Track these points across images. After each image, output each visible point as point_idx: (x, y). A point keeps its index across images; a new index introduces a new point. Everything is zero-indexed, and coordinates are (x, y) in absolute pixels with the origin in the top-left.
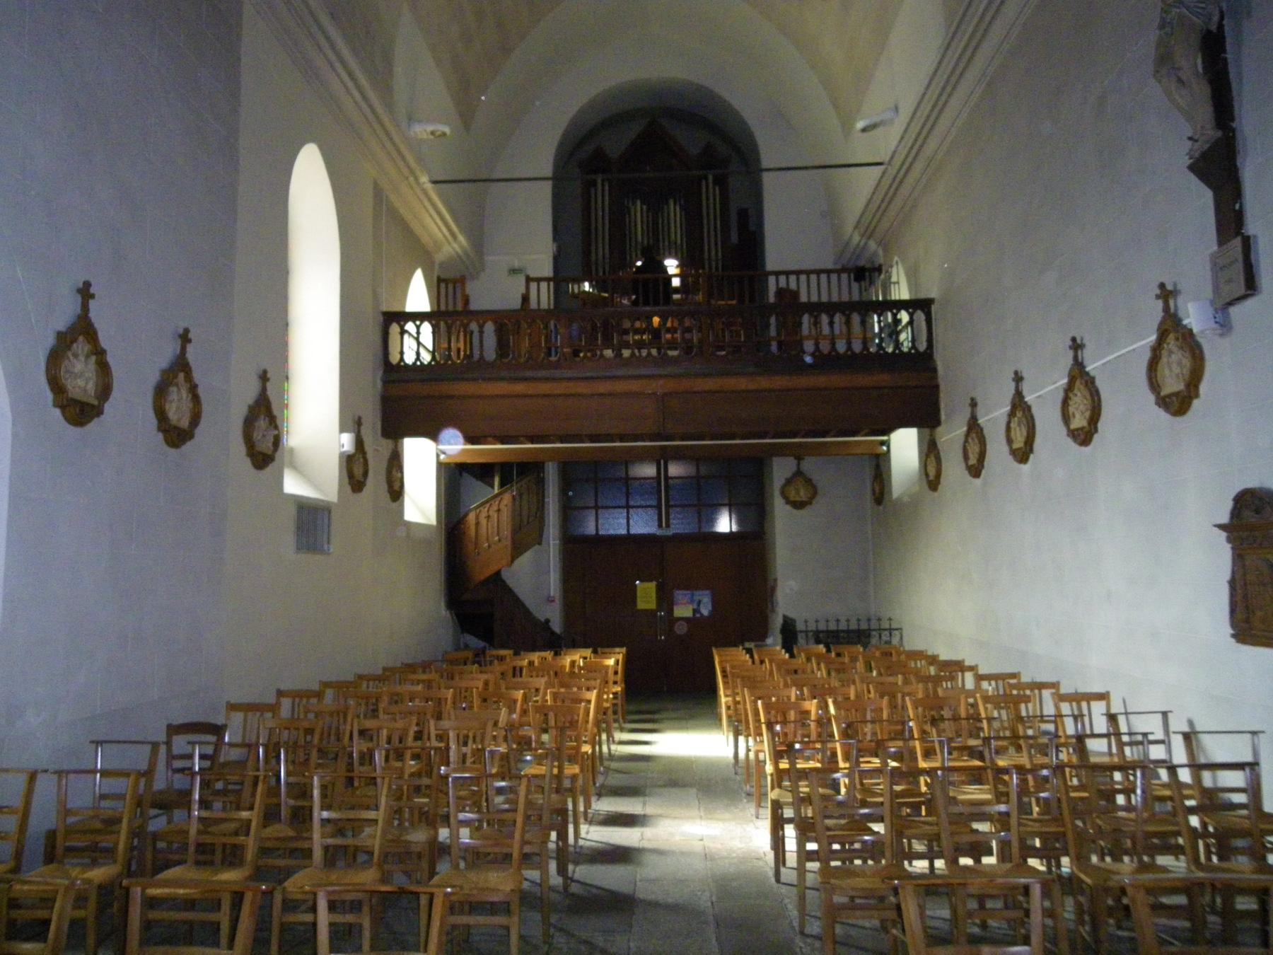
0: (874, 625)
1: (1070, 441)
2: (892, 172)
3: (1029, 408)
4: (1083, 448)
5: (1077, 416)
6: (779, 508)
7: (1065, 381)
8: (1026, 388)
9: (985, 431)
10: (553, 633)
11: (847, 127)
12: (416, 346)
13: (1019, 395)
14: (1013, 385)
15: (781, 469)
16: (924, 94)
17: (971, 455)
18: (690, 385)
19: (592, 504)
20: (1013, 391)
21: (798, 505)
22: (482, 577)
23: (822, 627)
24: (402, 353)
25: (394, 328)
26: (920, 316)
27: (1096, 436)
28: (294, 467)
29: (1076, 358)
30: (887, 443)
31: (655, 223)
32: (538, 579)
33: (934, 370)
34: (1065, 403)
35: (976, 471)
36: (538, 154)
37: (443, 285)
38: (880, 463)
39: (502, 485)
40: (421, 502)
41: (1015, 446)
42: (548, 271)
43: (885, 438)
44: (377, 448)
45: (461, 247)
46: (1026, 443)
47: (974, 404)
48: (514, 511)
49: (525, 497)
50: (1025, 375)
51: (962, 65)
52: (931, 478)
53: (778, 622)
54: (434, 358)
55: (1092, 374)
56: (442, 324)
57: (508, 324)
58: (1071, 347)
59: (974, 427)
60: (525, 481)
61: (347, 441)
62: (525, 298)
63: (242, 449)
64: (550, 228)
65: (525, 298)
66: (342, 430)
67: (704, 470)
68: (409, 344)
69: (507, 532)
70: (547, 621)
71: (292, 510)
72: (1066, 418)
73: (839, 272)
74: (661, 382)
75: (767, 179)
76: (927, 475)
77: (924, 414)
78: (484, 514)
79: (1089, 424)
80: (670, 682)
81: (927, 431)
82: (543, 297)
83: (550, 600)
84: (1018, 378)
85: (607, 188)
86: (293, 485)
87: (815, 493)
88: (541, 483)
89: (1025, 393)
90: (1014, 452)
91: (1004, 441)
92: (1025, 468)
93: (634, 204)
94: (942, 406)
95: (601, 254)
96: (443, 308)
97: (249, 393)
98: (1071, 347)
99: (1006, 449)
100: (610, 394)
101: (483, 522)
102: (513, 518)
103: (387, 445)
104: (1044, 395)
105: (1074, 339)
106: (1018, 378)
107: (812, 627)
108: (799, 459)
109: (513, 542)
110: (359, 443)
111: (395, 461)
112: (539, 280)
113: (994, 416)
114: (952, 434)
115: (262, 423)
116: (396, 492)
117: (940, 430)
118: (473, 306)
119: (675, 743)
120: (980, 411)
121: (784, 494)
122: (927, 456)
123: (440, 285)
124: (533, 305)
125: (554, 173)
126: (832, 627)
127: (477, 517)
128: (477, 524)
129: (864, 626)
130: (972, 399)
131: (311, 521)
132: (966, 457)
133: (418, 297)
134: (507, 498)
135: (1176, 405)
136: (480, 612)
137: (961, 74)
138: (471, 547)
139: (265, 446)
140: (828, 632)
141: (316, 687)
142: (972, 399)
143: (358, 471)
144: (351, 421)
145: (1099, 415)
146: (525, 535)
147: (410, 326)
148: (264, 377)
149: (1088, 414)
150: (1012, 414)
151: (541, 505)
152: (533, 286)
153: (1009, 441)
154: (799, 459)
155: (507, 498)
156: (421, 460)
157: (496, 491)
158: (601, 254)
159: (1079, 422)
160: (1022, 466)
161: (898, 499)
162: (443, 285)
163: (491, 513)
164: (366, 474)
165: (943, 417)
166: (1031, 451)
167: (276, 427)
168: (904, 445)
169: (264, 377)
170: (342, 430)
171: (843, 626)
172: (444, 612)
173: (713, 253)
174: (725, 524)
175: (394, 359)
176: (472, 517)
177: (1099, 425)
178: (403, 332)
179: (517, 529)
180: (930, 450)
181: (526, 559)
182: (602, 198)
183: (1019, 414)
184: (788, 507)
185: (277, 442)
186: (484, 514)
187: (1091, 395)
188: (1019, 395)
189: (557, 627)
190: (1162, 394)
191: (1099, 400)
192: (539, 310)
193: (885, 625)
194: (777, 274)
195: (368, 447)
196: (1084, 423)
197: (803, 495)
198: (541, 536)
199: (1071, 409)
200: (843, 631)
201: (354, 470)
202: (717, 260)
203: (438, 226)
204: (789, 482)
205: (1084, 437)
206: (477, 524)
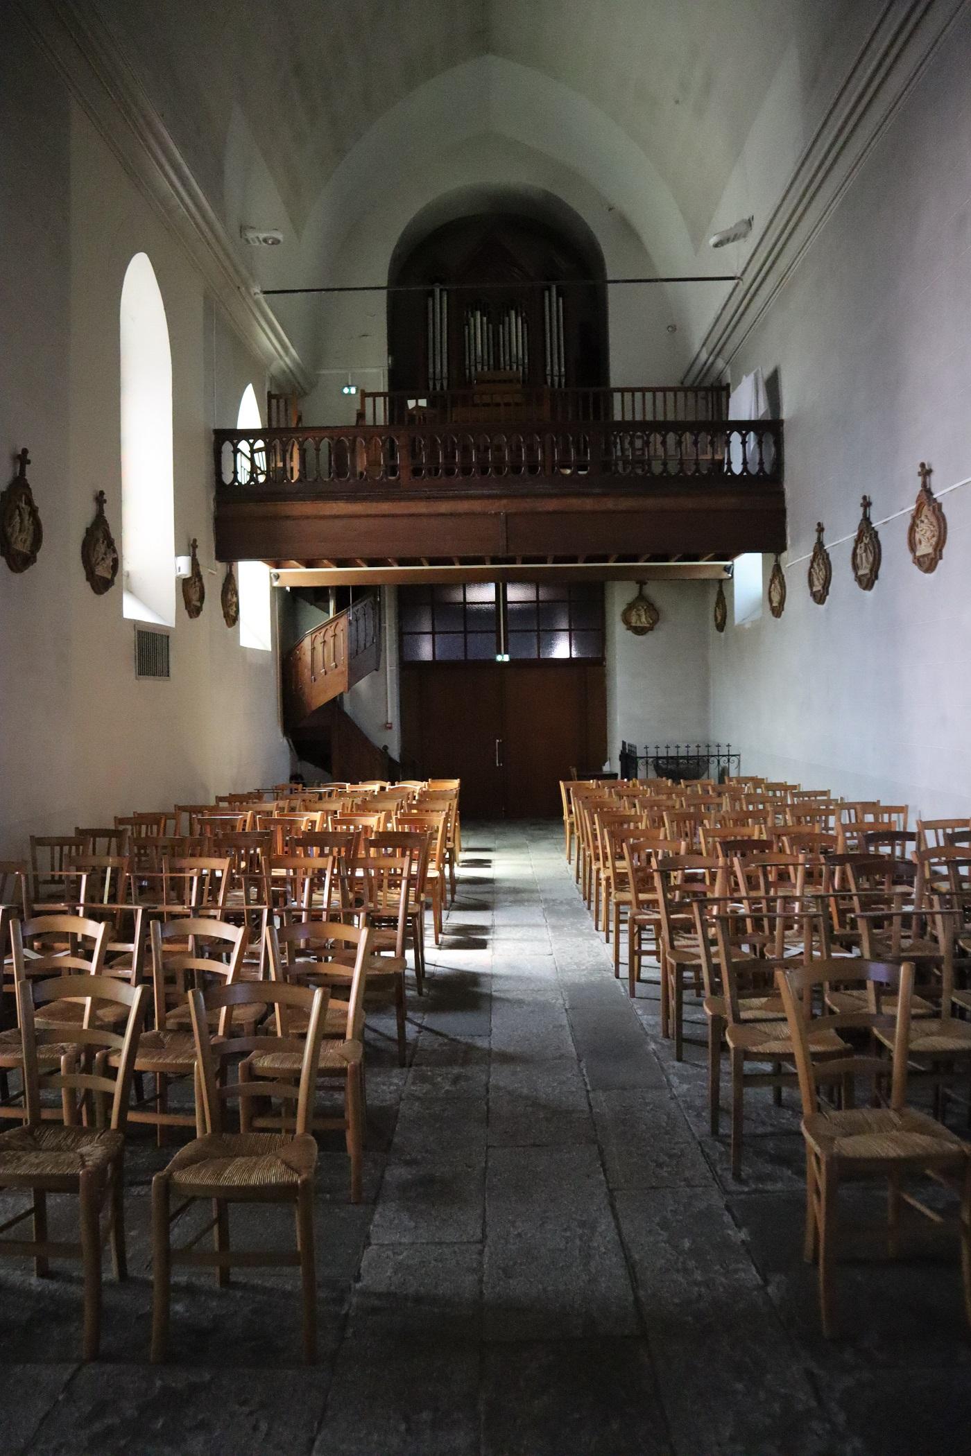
0: (714, 751)
1: (915, 568)
2: (743, 286)
3: (876, 533)
4: (927, 575)
5: (923, 543)
6: (619, 633)
7: (914, 507)
8: (935, 482)
9: (831, 557)
10: (391, 760)
11: (697, 238)
12: (246, 465)
13: (866, 520)
14: (815, 535)
15: (619, 597)
16: (780, 206)
17: (816, 582)
18: (537, 465)
19: (429, 629)
20: (861, 517)
21: (639, 631)
22: (314, 708)
23: (663, 753)
24: (235, 473)
25: (227, 447)
26: (769, 439)
27: (940, 562)
28: (131, 592)
29: (924, 484)
30: (728, 569)
31: (496, 334)
32: (379, 707)
33: (781, 494)
34: (912, 530)
35: (820, 597)
36: (377, 267)
37: (274, 402)
38: (722, 589)
39: (338, 609)
40: (256, 628)
41: (861, 572)
42: (383, 386)
43: (729, 563)
44: (213, 573)
45: (293, 360)
46: (871, 570)
47: (820, 529)
48: (350, 636)
49: (361, 622)
50: (872, 500)
51: (820, 175)
52: (775, 604)
53: (615, 750)
54: (235, 446)
55: (939, 500)
56: (277, 442)
57: (340, 443)
58: (920, 474)
59: (820, 555)
60: (359, 606)
61: (183, 566)
62: (361, 415)
63: (82, 574)
64: (384, 341)
65: (361, 415)
66: (177, 555)
67: (543, 595)
68: (244, 465)
69: (343, 657)
70: (386, 748)
71: (132, 636)
72: (913, 546)
73: (686, 390)
74: (504, 502)
75: (612, 291)
76: (771, 601)
77: (771, 541)
78: (320, 640)
79: (935, 550)
80: (510, 801)
81: (771, 556)
82: (379, 413)
83: (388, 727)
84: (866, 504)
85: (445, 298)
86: (132, 610)
87: (655, 621)
88: (378, 608)
89: (825, 542)
90: (859, 579)
91: (906, 547)
92: (868, 594)
93: (474, 316)
94: (788, 531)
95: (438, 370)
96: (274, 425)
97: (83, 516)
98: (920, 474)
99: (851, 575)
100: (451, 514)
101: (319, 647)
102: (350, 642)
103: (221, 568)
104: (892, 525)
105: (923, 465)
106: (866, 504)
107: (652, 753)
108: (642, 583)
109: (351, 668)
110: (195, 565)
111: (229, 586)
112: (375, 395)
113: (841, 544)
114: (797, 559)
115: (101, 548)
116: (231, 617)
117: (784, 555)
118: (306, 423)
119: (509, 863)
120: (826, 536)
121: (626, 621)
122: (772, 581)
123: (272, 401)
124: (369, 420)
125: (389, 281)
126: (672, 753)
127: (313, 643)
128: (313, 649)
129: (703, 752)
130: (819, 524)
131: (151, 650)
132: (811, 584)
133: (249, 415)
134: (343, 622)
135: (926, 566)
136: (319, 741)
137: (917, 25)
138: (307, 673)
139: (102, 571)
140: (667, 758)
141: (172, 810)
142: (819, 524)
143: (195, 597)
144: (187, 545)
145: (944, 542)
146: (361, 661)
147: (244, 446)
148: (100, 499)
149: (934, 540)
150: (858, 540)
151: (379, 630)
152: (369, 401)
153: (855, 567)
154: (642, 583)
155: (343, 622)
156: (256, 581)
157: (332, 616)
158: (438, 370)
159: (925, 549)
160: (867, 592)
161: (739, 626)
162: (274, 402)
163: (327, 642)
164: (202, 598)
165: (789, 542)
166: (876, 577)
167: (114, 551)
168: (748, 571)
169: (100, 499)
170: (177, 555)
171: (682, 752)
172: (283, 742)
173: (556, 368)
174: (562, 649)
175: (228, 479)
176: (307, 643)
177: (944, 551)
178: (236, 451)
179: (354, 654)
180: (775, 576)
181: (363, 684)
182: (439, 307)
183: (866, 541)
184: (630, 633)
185: (116, 565)
186: (320, 640)
187: (938, 519)
188: (866, 520)
189: (395, 753)
190: (918, 554)
191: (945, 528)
192: (375, 426)
193: (724, 751)
194: (622, 391)
195: (204, 572)
196: (930, 550)
197: (644, 621)
198: (378, 663)
199: (918, 536)
200: (683, 757)
201: (191, 593)
202: (560, 376)
203: (274, 344)
204: (631, 606)
205: (928, 564)
206: (313, 649)
